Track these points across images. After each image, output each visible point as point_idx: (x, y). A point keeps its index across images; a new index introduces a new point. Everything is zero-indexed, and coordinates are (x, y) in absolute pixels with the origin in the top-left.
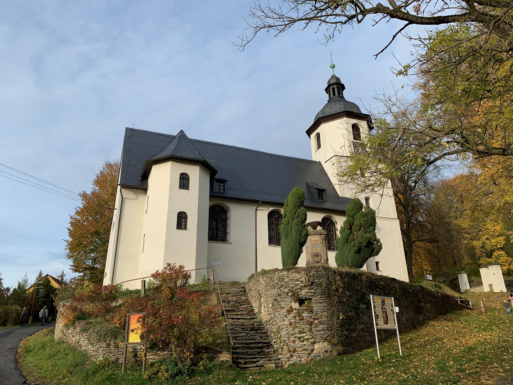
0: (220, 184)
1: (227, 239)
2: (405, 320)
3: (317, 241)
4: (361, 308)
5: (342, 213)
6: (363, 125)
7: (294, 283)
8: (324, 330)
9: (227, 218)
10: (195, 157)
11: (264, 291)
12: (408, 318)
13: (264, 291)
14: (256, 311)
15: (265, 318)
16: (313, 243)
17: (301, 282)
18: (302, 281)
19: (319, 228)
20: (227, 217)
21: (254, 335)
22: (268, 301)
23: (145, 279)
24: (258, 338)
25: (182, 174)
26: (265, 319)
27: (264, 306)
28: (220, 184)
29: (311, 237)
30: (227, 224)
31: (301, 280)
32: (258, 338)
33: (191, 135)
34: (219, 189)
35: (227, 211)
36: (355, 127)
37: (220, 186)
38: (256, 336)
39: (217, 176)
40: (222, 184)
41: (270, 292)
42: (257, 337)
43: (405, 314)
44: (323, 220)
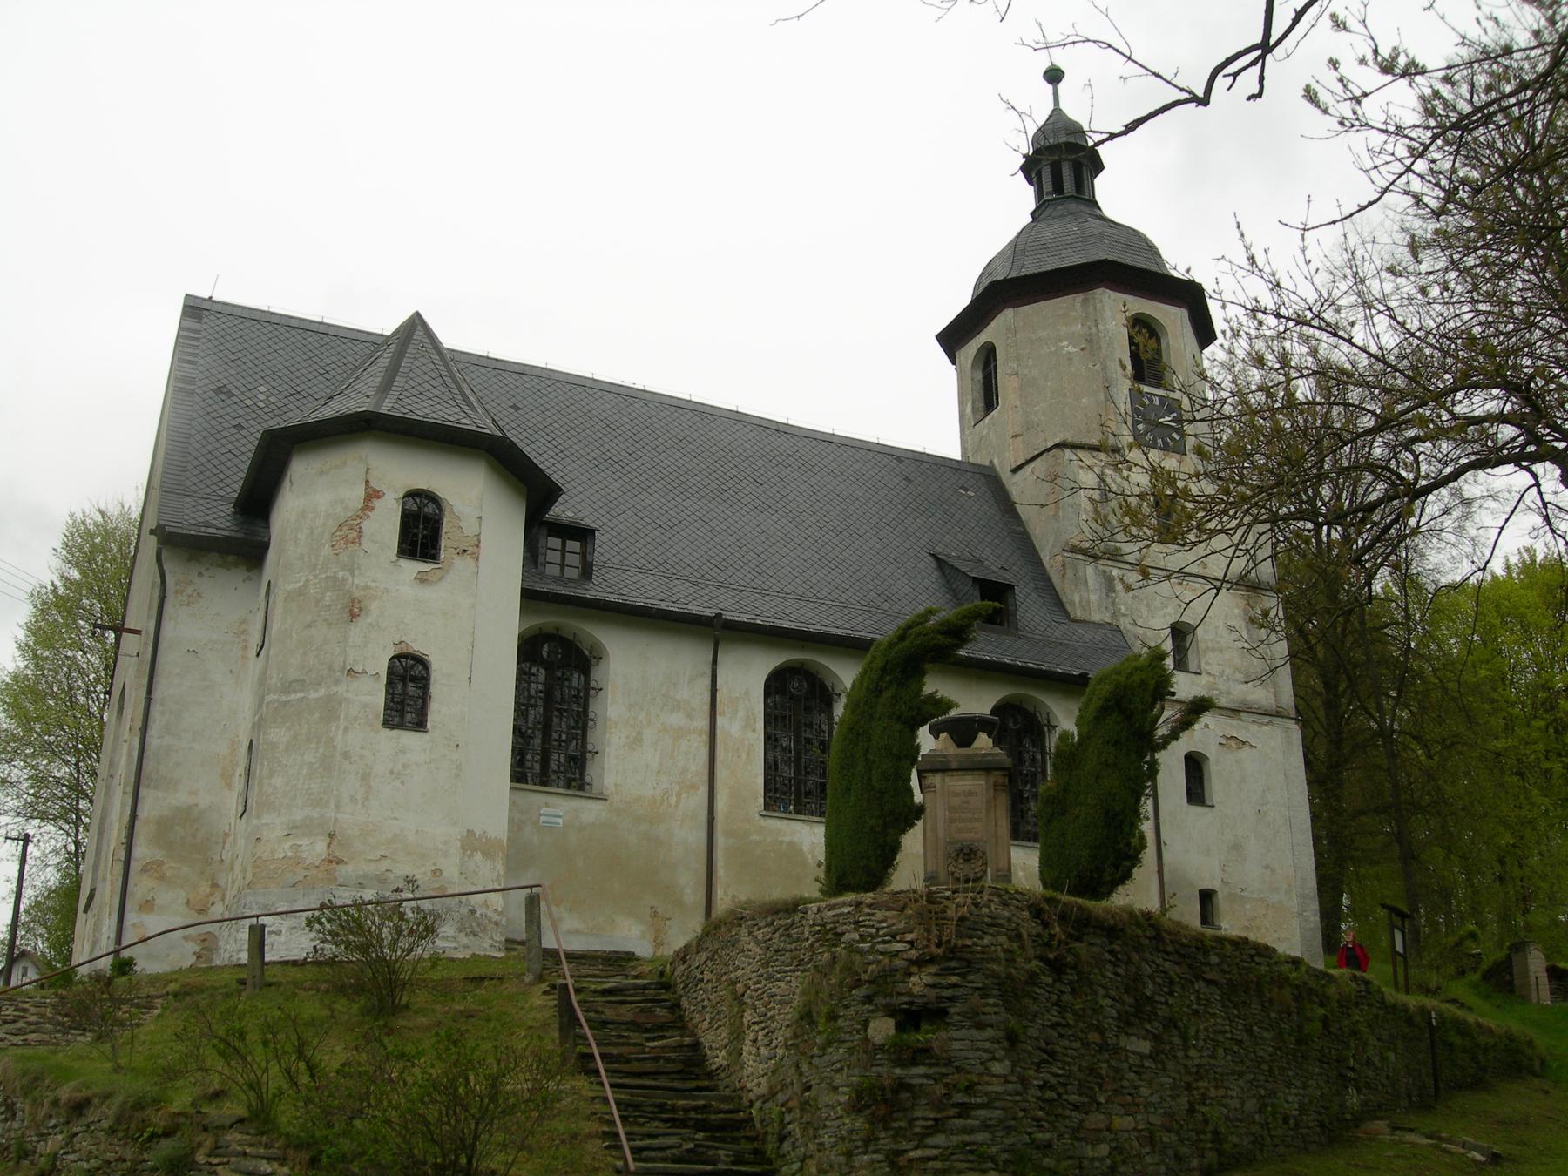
0: (564, 545)
1: (588, 779)
2: (1296, 1106)
3: (970, 793)
4: (1134, 1053)
5: (1071, 684)
6: (1173, 319)
7: (880, 947)
8: (990, 1126)
9: (592, 692)
10: (465, 421)
11: (755, 984)
12: (1306, 1100)
13: (755, 984)
14: (719, 1059)
15: (759, 1085)
16: (956, 801)
17: (908, 946)
18: (911, 942)
19: (983, 742)
20: (593, 684)
21: (710, 1147)
22: (772, 1017)
23: (262, 920)
24: (727, 1156)
25: (413, 494)
26: (755, 1089)
27: (755, 1041)
28: (564, 545)
29: (947, 779)
30: (591, 715)
31: (909, 937)
32: (727, 1156)
33: (454, 335)
34: (562, 566)
35: (593, 661)
36: (1142, 325)
37: (563, 551)
38: (717, 1148)
39: (562, 511)
40: (574, 546)
41: (782, 984)
42: (721, 1152)
43: (1298, 1084)
44: (996, 710)
